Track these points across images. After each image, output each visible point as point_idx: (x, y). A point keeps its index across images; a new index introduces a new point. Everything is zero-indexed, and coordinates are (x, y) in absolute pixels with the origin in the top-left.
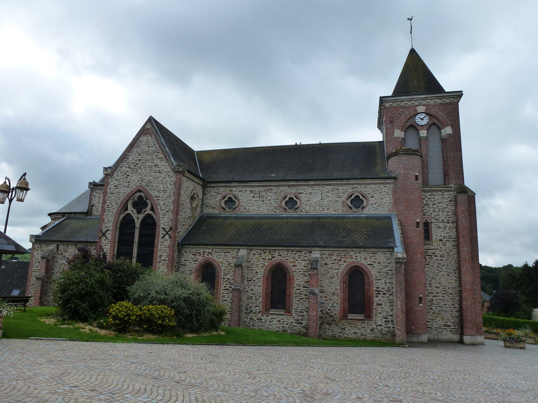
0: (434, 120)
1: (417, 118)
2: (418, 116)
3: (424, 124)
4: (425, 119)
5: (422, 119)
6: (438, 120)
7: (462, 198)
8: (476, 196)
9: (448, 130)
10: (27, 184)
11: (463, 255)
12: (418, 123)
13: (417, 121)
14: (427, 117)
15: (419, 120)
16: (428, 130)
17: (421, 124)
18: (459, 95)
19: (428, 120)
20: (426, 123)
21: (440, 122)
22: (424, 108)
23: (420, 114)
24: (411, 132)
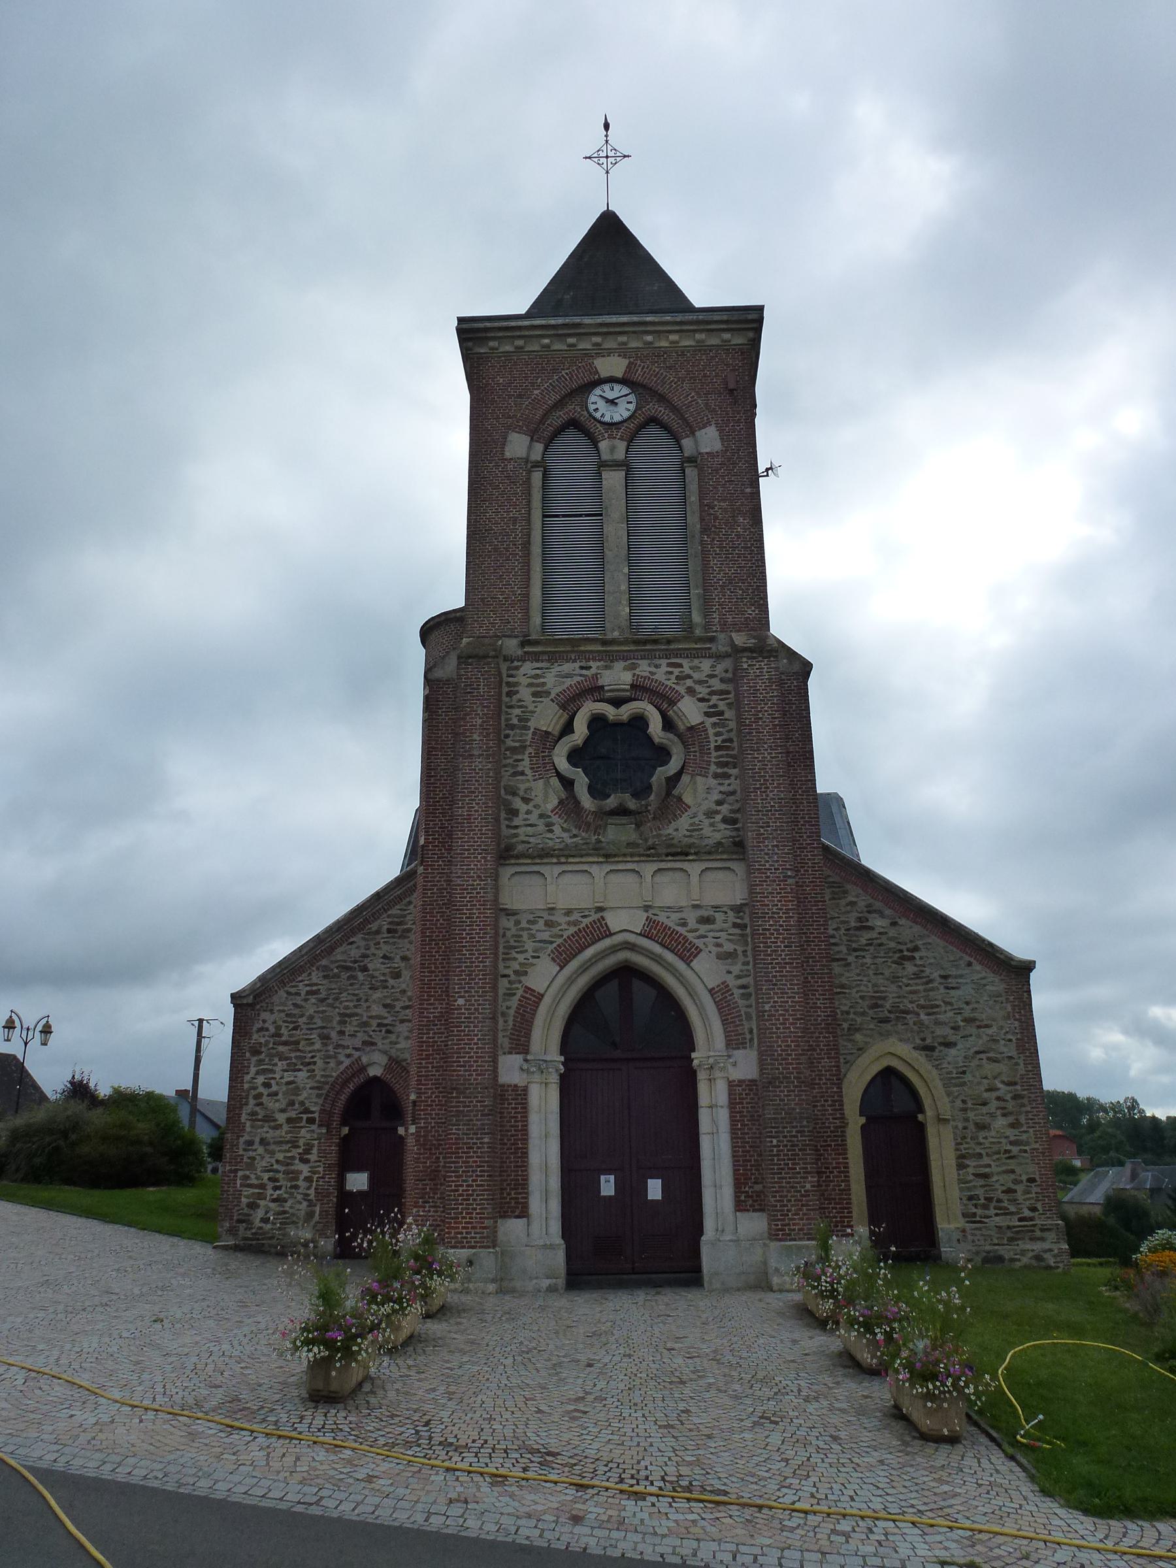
0: (655, 408)
1: (592, 398)
2: (598, 391)
3: (617, 418)
4: (622, 404)
5: (612, 402)
6: (674, 409)
7: (759, 671)
8: (812, 683)
9: (709, 440)
10: (50, 1027)
11: (790, 1295)
12: (598, 415)
13: (592, 407)
14: (632, 398)
15: (601, 404)
16: (630, 441)
17: (607, 419)
18: (747, 322)
19: (632, 407)
20: (626, 414)
21: (674, 409)
22: (625, 362)
23: (606, 387)
24: (571, 441)
